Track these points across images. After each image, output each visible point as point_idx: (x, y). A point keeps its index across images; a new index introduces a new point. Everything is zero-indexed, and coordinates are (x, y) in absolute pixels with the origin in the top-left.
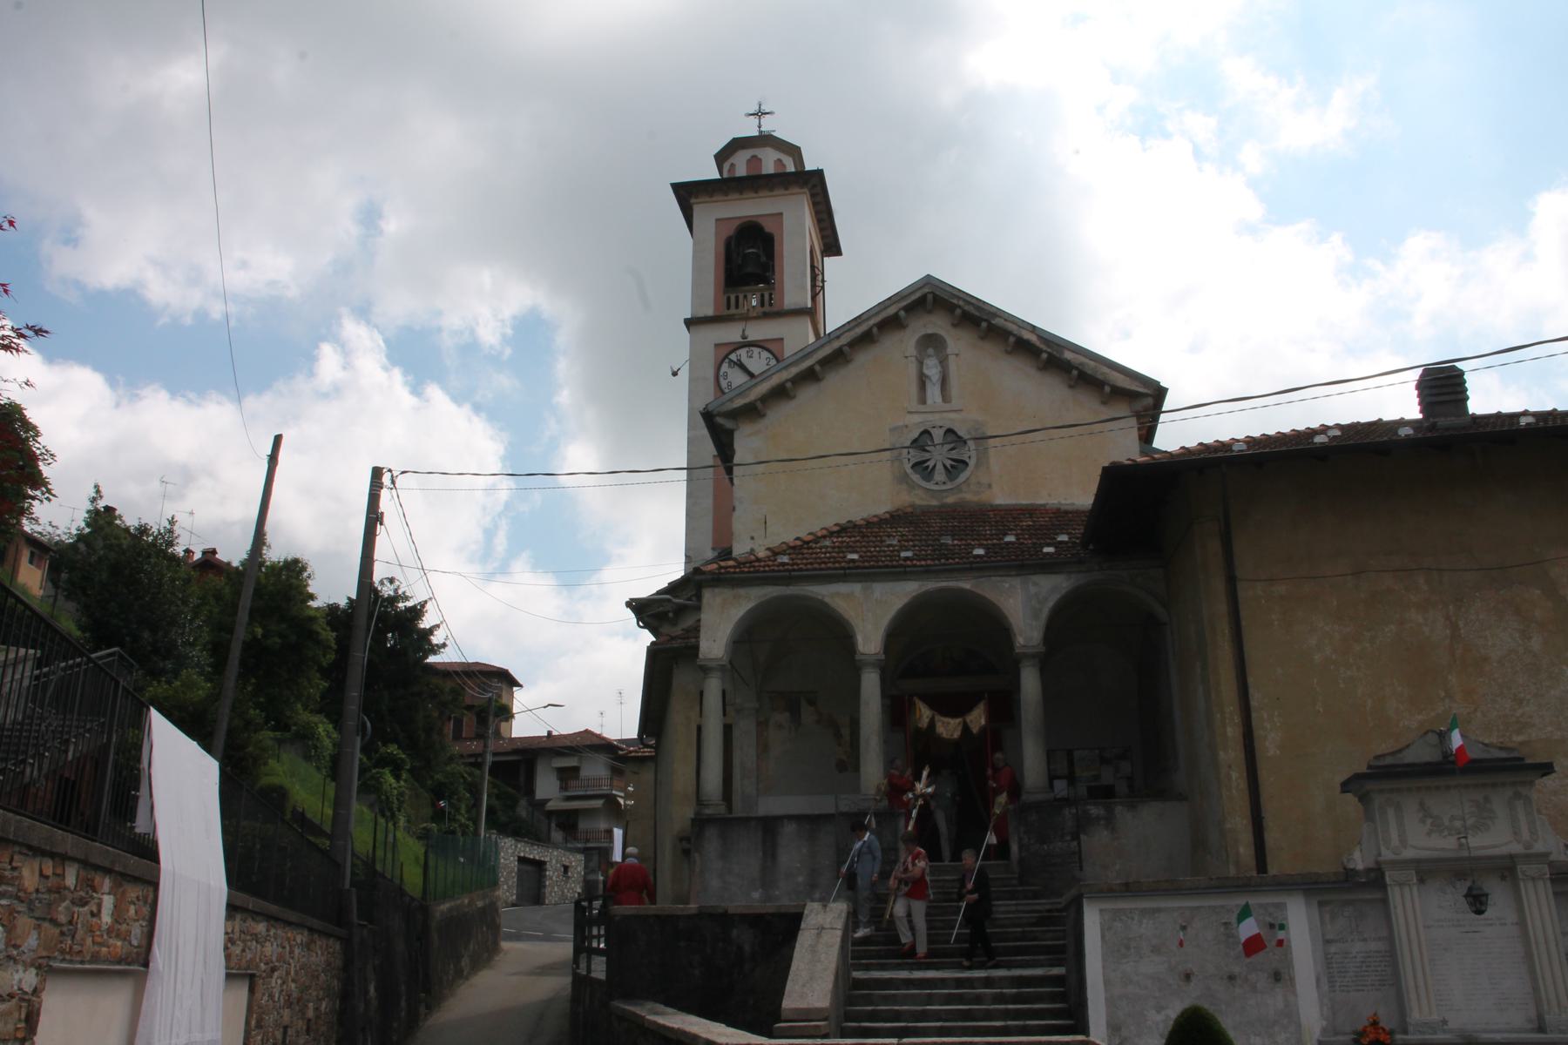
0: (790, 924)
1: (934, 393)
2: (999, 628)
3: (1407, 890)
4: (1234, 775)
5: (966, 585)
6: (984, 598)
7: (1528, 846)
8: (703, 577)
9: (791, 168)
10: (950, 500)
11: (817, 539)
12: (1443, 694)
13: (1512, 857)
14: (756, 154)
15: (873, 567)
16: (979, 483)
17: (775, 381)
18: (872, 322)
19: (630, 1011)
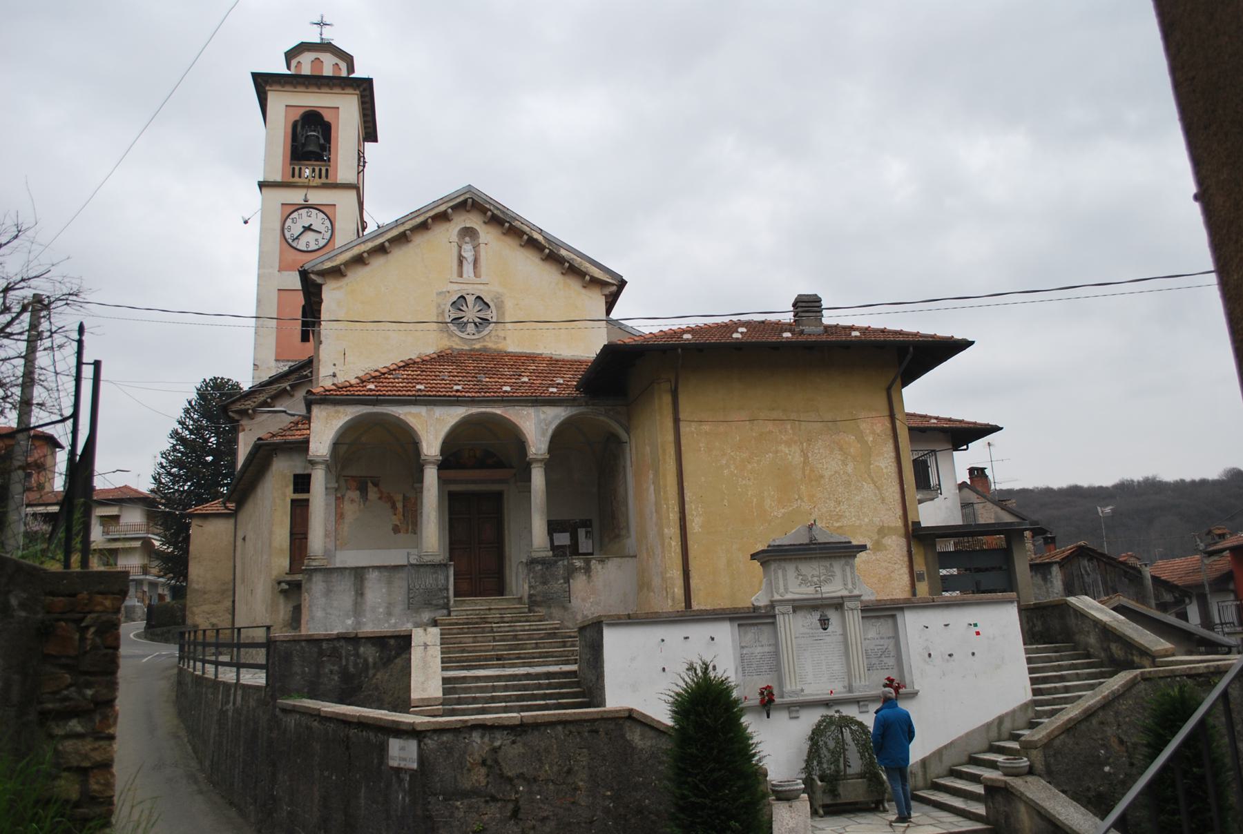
0: (404, 642)
1: (468, 268)
2: (519, 442)
3: (786, 616)
4: (673, 544)
5: (498, 411)
6: (509, 420)
7: (851, 591)
8: (314, 397)
9: (344, 74)
10: (477, 346)
11: (390, 372)
12: (797, 497)
13: (842, 597)
14: (319, 57)
15: (435, 396)
16: (497, 336)
17: (356, 251)
18: (428, 215)
19: (286, 704)
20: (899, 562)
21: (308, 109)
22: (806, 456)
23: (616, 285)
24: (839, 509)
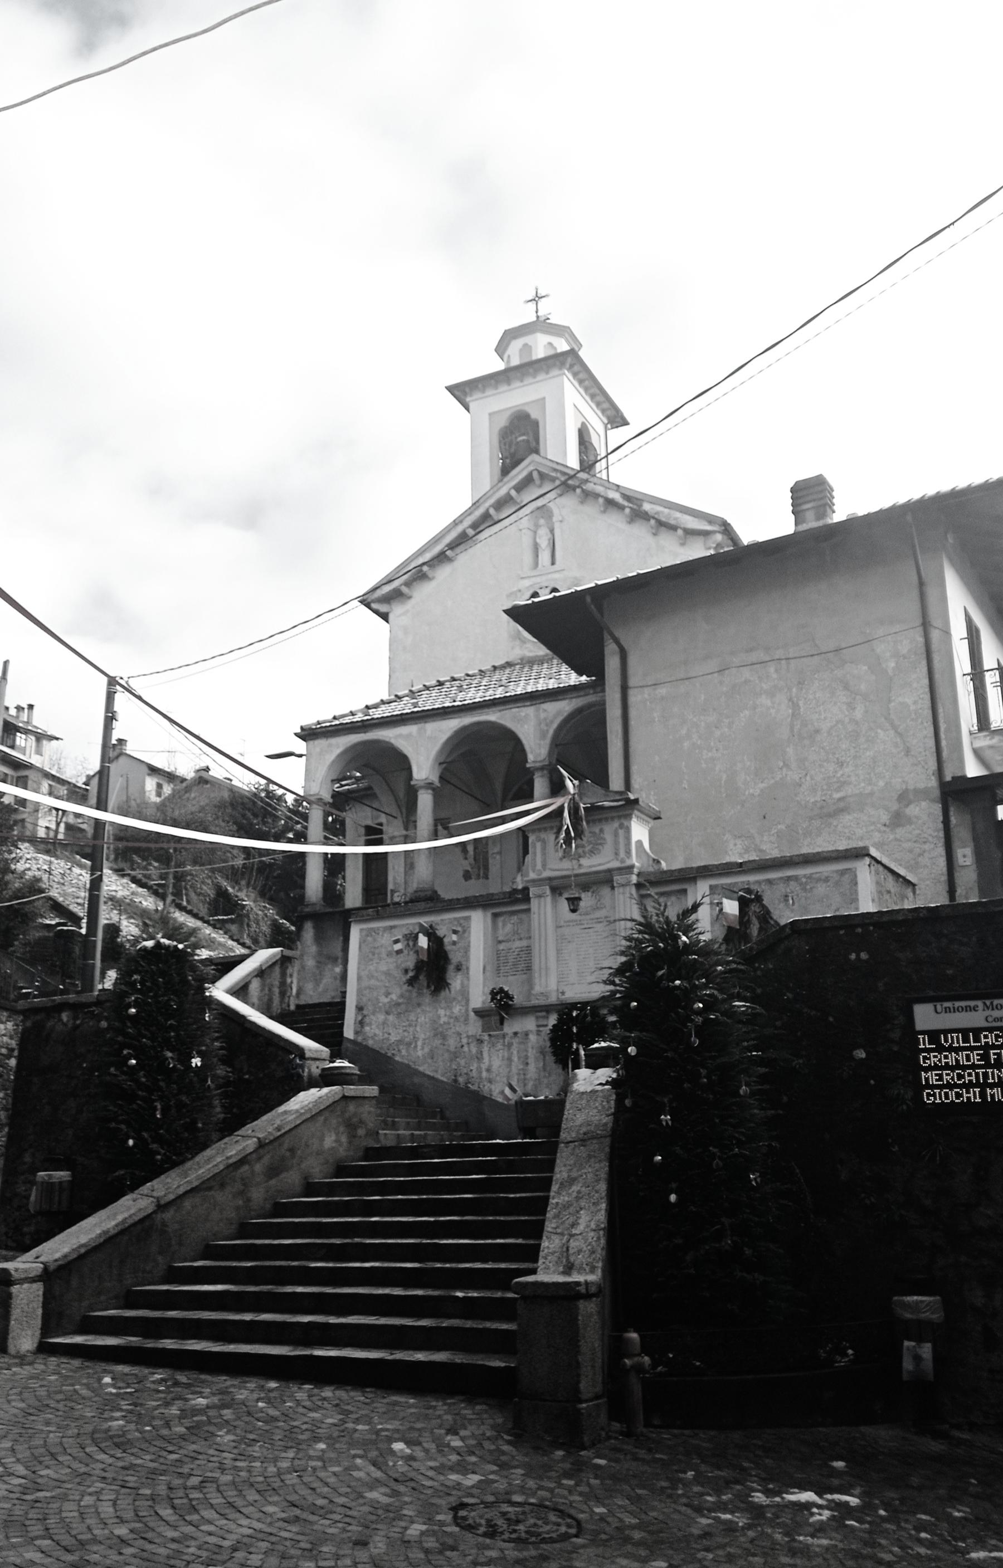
7: (623, 861)
12: (781, 764)
13: (610, 871)
18: (487, 504)
20: (930, 839)
21: (513, 410)
22: (795, 706)
23: (719, 532)
24: (841, 772)
